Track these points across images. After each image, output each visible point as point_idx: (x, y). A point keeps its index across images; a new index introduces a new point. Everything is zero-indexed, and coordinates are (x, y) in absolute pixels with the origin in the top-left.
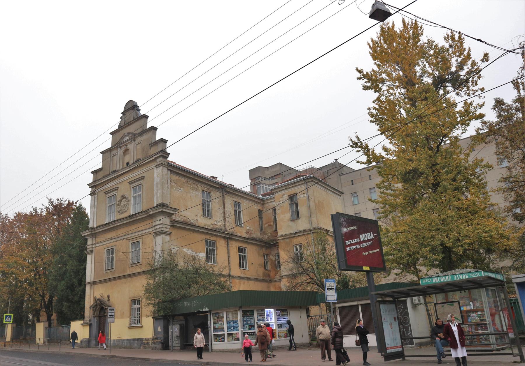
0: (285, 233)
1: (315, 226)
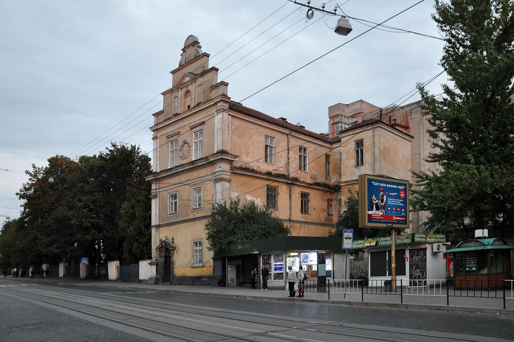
0: (348, 180)
1: (377, 173)
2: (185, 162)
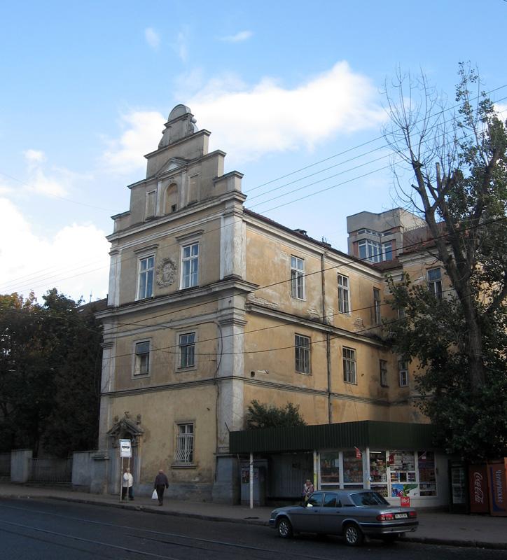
2: (165, 291)
